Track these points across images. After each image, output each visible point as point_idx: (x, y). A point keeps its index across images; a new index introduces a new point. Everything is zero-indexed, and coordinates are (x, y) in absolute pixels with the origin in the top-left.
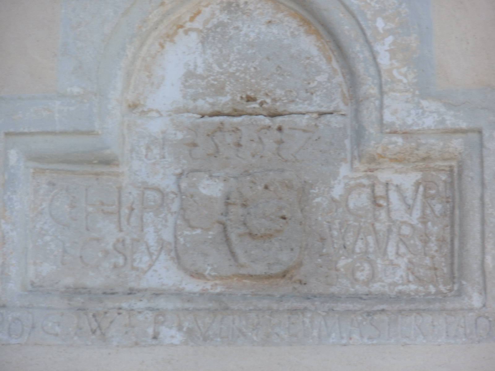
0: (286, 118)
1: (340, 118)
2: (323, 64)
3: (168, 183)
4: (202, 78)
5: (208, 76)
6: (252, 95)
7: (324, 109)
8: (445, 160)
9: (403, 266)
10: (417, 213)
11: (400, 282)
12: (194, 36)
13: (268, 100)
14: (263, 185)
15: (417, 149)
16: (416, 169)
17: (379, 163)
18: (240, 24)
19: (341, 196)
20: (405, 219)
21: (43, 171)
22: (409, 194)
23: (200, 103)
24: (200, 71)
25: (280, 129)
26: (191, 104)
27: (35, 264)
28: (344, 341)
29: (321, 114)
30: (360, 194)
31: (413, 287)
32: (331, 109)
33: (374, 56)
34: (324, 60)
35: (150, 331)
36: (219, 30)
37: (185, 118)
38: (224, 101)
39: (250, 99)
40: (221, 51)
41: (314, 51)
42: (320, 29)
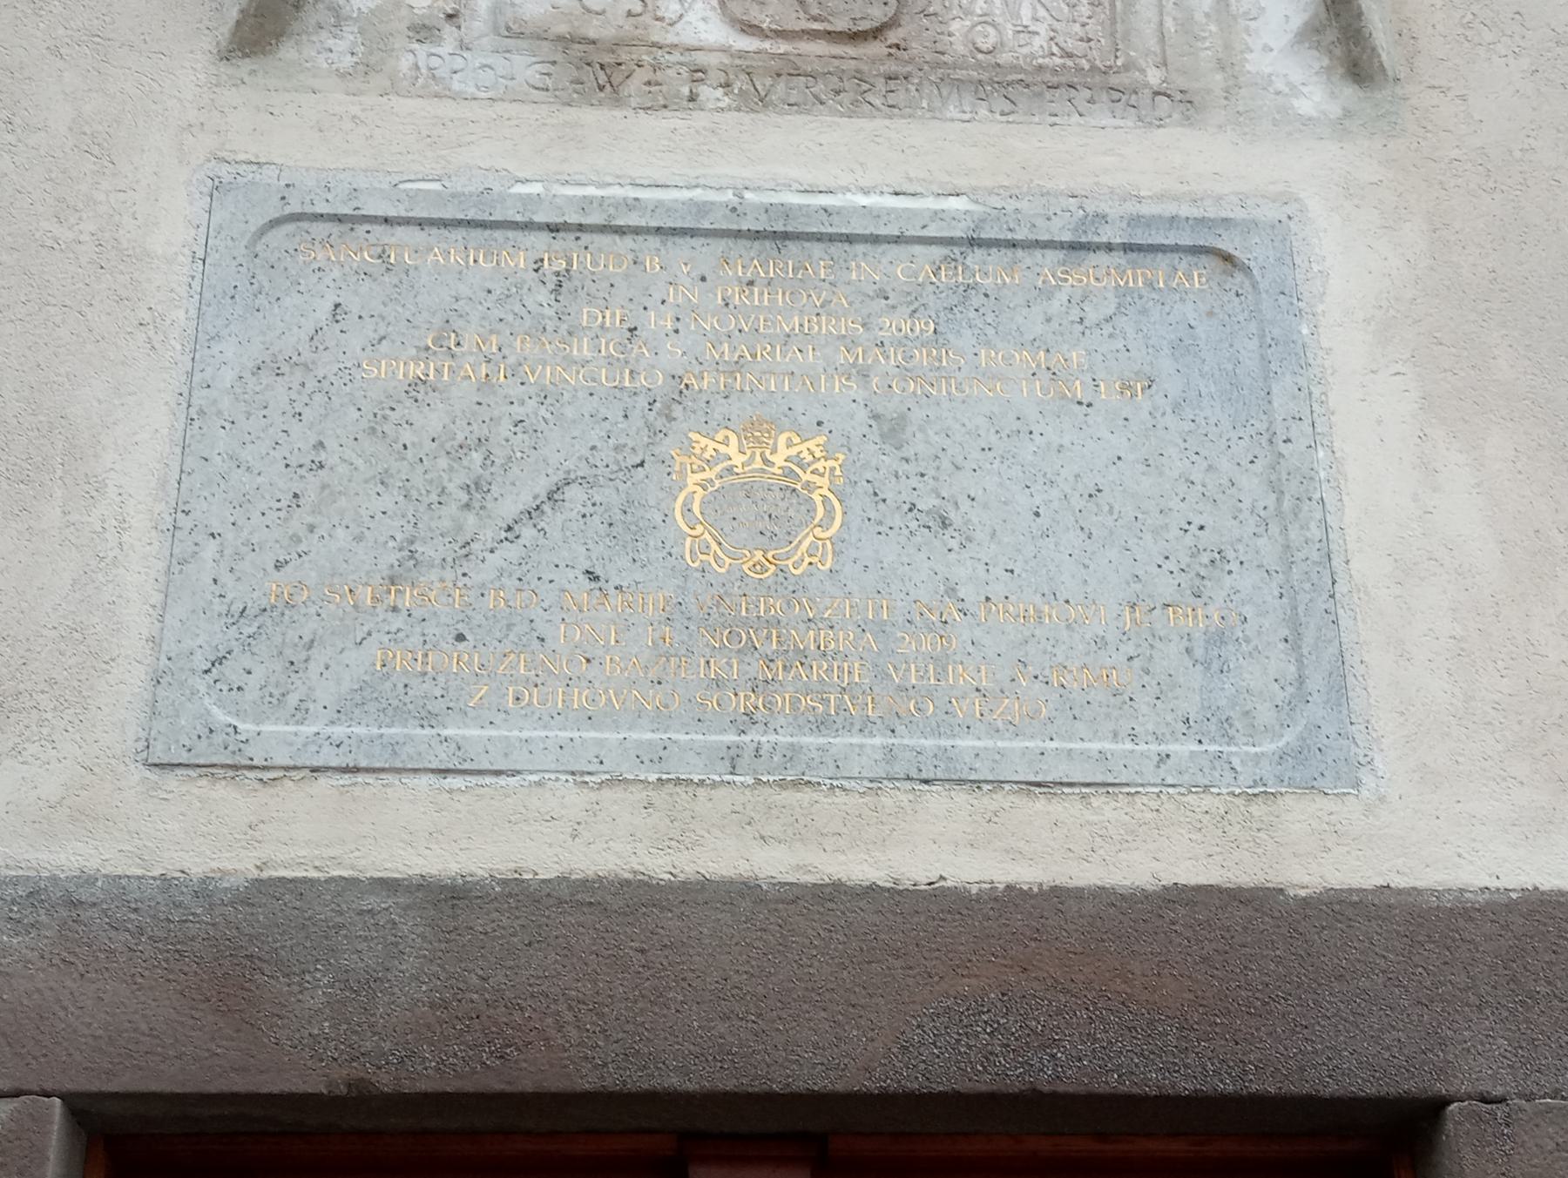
28: (967, 117)
31: (1058, 61)
35: (686, 91)
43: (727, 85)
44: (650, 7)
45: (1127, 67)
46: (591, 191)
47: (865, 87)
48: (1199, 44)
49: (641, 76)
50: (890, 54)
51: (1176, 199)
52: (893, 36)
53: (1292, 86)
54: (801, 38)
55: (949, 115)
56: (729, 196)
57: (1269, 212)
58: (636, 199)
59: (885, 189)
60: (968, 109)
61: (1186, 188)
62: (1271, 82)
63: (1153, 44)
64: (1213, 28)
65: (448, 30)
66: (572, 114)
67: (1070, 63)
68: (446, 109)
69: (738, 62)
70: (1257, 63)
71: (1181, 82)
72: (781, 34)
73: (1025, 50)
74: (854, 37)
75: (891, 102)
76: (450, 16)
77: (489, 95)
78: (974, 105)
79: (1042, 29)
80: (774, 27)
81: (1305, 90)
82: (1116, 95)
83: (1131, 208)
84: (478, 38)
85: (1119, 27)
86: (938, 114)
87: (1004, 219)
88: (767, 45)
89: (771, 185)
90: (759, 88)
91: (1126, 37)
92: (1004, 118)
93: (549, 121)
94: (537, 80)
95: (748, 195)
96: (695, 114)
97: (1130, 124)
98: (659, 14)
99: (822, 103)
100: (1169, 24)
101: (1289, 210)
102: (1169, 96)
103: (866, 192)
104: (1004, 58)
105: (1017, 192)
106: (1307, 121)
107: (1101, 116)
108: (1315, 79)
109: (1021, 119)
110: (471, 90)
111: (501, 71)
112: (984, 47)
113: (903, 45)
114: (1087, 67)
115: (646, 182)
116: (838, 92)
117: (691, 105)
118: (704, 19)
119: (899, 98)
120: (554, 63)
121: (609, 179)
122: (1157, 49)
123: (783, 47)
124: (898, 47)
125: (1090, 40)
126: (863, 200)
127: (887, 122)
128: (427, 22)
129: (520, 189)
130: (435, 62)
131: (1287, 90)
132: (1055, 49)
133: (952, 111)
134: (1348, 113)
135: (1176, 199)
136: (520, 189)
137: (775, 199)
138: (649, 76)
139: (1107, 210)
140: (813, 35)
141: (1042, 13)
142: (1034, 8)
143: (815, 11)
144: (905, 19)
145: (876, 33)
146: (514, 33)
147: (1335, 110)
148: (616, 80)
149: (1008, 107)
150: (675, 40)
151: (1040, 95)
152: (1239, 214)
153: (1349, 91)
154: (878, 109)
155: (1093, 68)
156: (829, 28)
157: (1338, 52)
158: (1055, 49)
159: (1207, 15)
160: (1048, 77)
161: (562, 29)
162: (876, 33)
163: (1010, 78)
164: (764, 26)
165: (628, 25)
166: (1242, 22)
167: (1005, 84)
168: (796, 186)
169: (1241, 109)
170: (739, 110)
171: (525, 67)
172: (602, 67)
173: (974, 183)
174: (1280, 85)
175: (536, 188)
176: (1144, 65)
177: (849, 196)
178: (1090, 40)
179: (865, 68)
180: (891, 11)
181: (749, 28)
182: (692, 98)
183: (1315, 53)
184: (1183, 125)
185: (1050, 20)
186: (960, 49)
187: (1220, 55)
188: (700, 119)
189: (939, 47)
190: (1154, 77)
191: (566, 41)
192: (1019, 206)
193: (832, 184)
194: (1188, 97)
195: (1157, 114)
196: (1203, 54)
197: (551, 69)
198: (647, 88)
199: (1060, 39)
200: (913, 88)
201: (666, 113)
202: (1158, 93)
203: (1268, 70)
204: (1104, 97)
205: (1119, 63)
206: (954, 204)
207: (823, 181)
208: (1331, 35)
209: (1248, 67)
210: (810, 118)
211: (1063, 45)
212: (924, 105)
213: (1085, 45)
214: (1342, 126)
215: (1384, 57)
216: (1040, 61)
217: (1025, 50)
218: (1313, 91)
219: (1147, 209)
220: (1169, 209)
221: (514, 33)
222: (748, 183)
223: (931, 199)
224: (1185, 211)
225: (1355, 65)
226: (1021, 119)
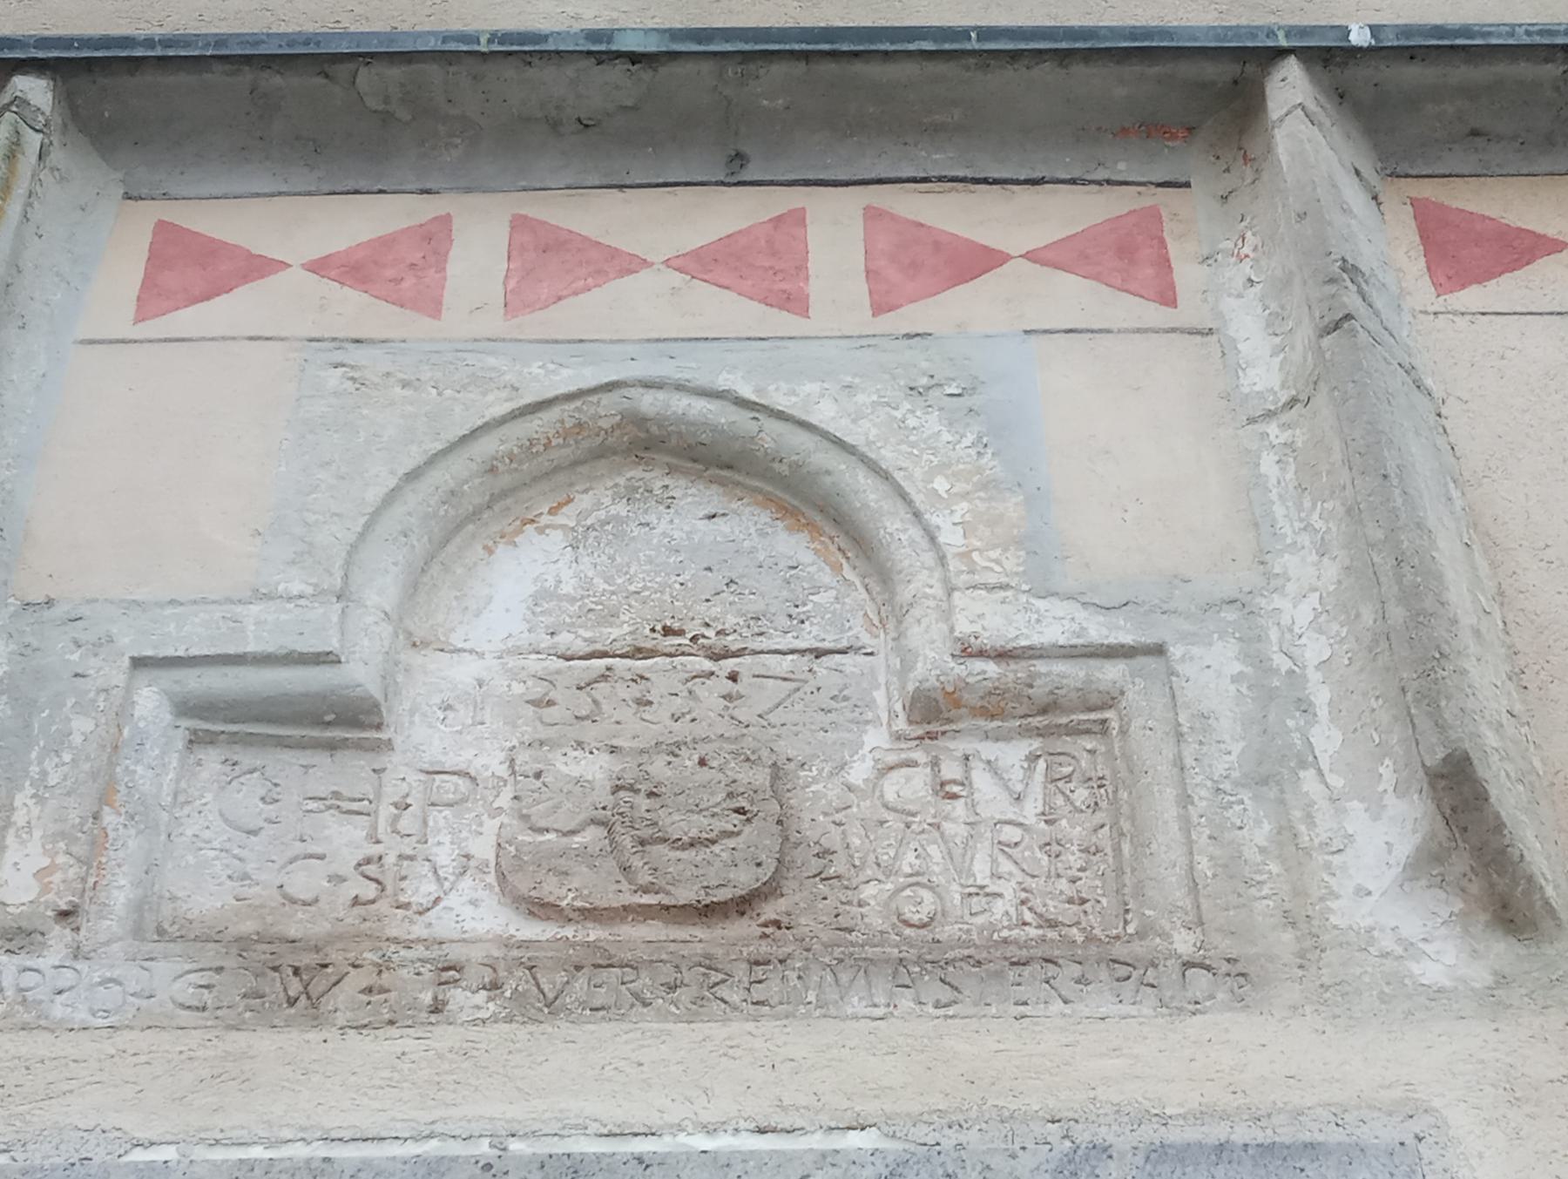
0: (748, 660)
1: (860, 659)
2: (827, 577)
3: (491, 763)
4: (573, 600)
5: (582, 597)
6: (676, 626)
7: (827, 645)
8: (1090, 710)
9: (1009, 894)
10: (1031, 810)
11: (1006, 923)
12: (557, 536)
13: (710, 633)
14: (696, 758)
15: (1031, 686)
16: (1027, 732)
17: (949, 721)
18: (652, 518)
19: (866, 780)
20: (1010, 816)
21: (210, 739)
22: (1017, 775)
23: (565, 640)
24: (567, 588)
25: (733, 677)
26: (546, 642)
27: (138, 762)
28: (879, 1012)
29: (819, 654)
30: (908, 779)
31: (1033, 932)
32: (844, 644)
33: (931, 537)
34: (827, 569)
35: (427, 998)
36: (609, 527)
37: (533, 663)
38: (617, 633)
39: (668, 631)
40: (612, 558)
41: (806, 557)
42: (818, 518)
43: (495, 986)
44: (389, 890)
45: (1141, 935)
46: (257, 1152)
47: (716, 977)
48: (1253, 891)
49: (357, 980)
50: (765, 936)
51: (1225, 1116)
52: (770, 911)
53: (1408, 945)
54: (623, 920)
55: (850, 1011)
56: (483, 1148)
57: (1381, 1132)
58: (326, 1160)
59: (742, 1124)
60: (881, 1000)
61: (1241, 1100)
62: (1372, 941)
63: (1180, 896)
64: (1274, 868)
65: (59, 936)
66: (240, 1040)
67: (1052, 934)
68: (38, 1045)
69: (515, 953)
70: (1346, 913)
71: (1226, 946)
72: (590, 914)
73: (979, 920)
74: (707, 912)
75: (756, 997)
76: (64, 914)
77: (106, 1022)
78: (891, 995)
79: (1008, 889)
80: (578, 904)
81: (1429, 948)
82: (1123, 971)
83: (1150, 1133)
84: (107, 943)
85: (1127, 879)
86: (833, 1011)
87: (937, 1160)
88: (569, 932)
89: (554, 1127)
90: (546, 988)
91: (1139, 892)
92: (941, 1012)
93: (199, 1053)
94: (189, 995)
95: (515, 1146)
96: (438, 1030)
97: (1146, 1011)
98: (403, 899)
99: (646, 1004)
100: (1203, 865)
101: (1416, 1126)
102: (1208, 968)
103: (710, 1130)
104: (947, 932)
105: (961, 1118)
106: (1438, 993)
107: (1100, 1000)
108: (1443, 931)
109: (972, 1011)
110: (82, 1015)
111: (132, 987)
112: (915, 918)
113: (785, 920)
114: (1080, 939)
115: (347, 1135)
116: (672, 988)
117: (433, 1018)
118: (474, 903)
119: (771, 989)
120: (219, 970)
121: (287, 1134)
122: (1188, 903)
123: (595, 933)
124: (777, 924)
125: (1083, 901)
126: (702, 1142)
127: (750, 1026)
128: (24, 924)
129: (139, 1156)
130: (29, 979)
131: (1399, 950)
132: (1028, 917)
133: (855, 1004)
134: (1502, 980)
135: (1225, 1116)
136: (139, 1156)
137: (559, 1147)
138: (372, 979)
139: (1111, 1139)
140: (644, 913)
141: (1006, 866)
142: (994, 861)
143: (645, 878)
144: (789, 886)
145: (743, 905)
146: (157, 930)
147: (1480, 975)
148: (315, 990)
149: (946, 994)
150: (424, 933)
151: (999, 975)
152: (1334, 1136)
153: (1501, 950)
154: (736, 1008)
155: (1090, 939)
156: (666, 901)
157: (1474, 888)
158: (1028, 917)
159: (1262, 850)
160: (1012, 951)
161: (248, 927)
162: (743, 905)
163: (950, 955)
164: (563, 904)
165: (352, 917)
166: (1321, 858)
167: (938, 964)
168: (594, 1127)
169: (1326, 980)
170: (509, 1019)
171: (173, 979)
172: (296, 972)
173: (888, 1108)
174: (1388, 943)
175: (169, 1153)
176: (1168, 927)
177: (682, 1138)
178: (1083, 901)
179: (719, 952)
180: (766, 873)
181: (541, 909)
182: (437, 1008)
183: (1442, 895)
184: (1231, 1009)
185: (1020, 876)
186: (877, 922)
187: (1287, 906)
188: (445, 1037)
189: (843, 921)
190: (1184, 942)
191: (243, 944)
192: (963, 1138)
193: (655, 1120)
194: (1239, 968)
195: (1189, 994)
196: (1260, 906)
197: (215, 978)
198: (365, 998)
199: (1036, 902)
200: (793, 975)
201: (393, 1031)
202: (1188, 965)
203: (1368, 922)
204: (1104, 974)
205: (1130, 930)
206: (854, 1140)
207: (637, 1115)
208: (1460, 863)
209: (1333, 920)
210: (625, 1026)
211: (1041, 910)
212: (811, 997)
213: (1075, 908)
214: (1495, 998)
215: (1550, 891)
216: (1005, 933)
217: (979, 920)
218: (1442, 949)
219: (1176, 1135)
220: (1217, 1132)
221: (157, 930)
222: (516, 1127)
223: (818, 1136)
224: (1242, 1134)
225: (1504, 907)
226: (972, 1011)
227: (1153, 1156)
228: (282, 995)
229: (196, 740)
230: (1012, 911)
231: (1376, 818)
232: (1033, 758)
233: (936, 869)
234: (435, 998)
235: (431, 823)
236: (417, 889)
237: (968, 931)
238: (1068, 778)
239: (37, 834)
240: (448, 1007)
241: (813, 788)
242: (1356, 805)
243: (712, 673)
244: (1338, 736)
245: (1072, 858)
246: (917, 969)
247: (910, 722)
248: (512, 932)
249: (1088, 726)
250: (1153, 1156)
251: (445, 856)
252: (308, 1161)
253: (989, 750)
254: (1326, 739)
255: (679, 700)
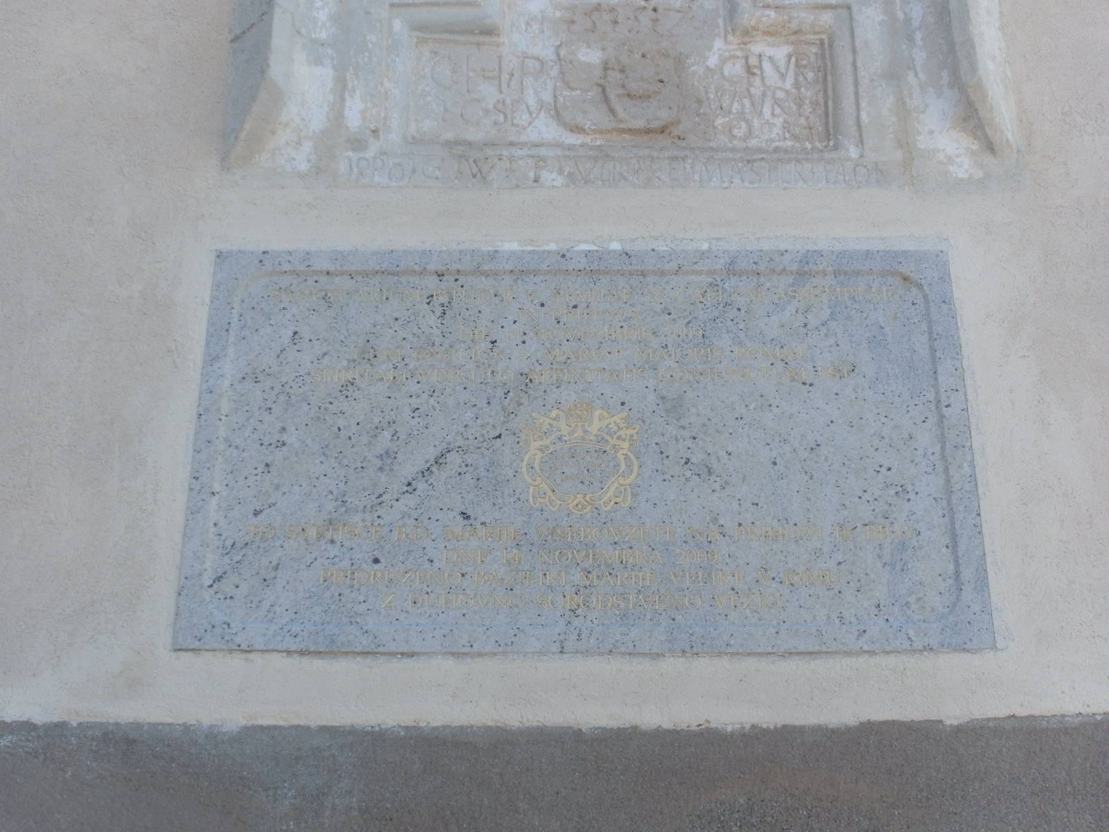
3: (548, 53)
8: (816, 33)
9: (779, 125)
17: (753, 36)
30: (734, 64)
31: (789, 143)
79: (779, 122)
88: (588, 139)
90: (582, 170)
117: (535, 185)
141: (778, 111)
158: (787, 135)
170: (568, 186)
227: (840, 255)
228: (470, 172)
229: (421, 42)
230: (780, 133)
231: (939, 97)
232: (789, 56)
233: (747, 111)
234: (535, 175)
235: (524, 84)
236: (521, 117)
237: (761, 142)
238: (805, 67)
239: (358, 93)
240: (541, 179)
241: (692, 68)
242: (931, 89)
243: (645, 8)
244: (924, 54)
245: (806, 107)
246: (741, 165)
247: (914, 285)
248: (564, 139)
249: (814, 41)
250: (840, 255)
251: (531, 101)
252: (489, 252)
253: (769, 51)
254: (920, 56)
255: (631, 22)
